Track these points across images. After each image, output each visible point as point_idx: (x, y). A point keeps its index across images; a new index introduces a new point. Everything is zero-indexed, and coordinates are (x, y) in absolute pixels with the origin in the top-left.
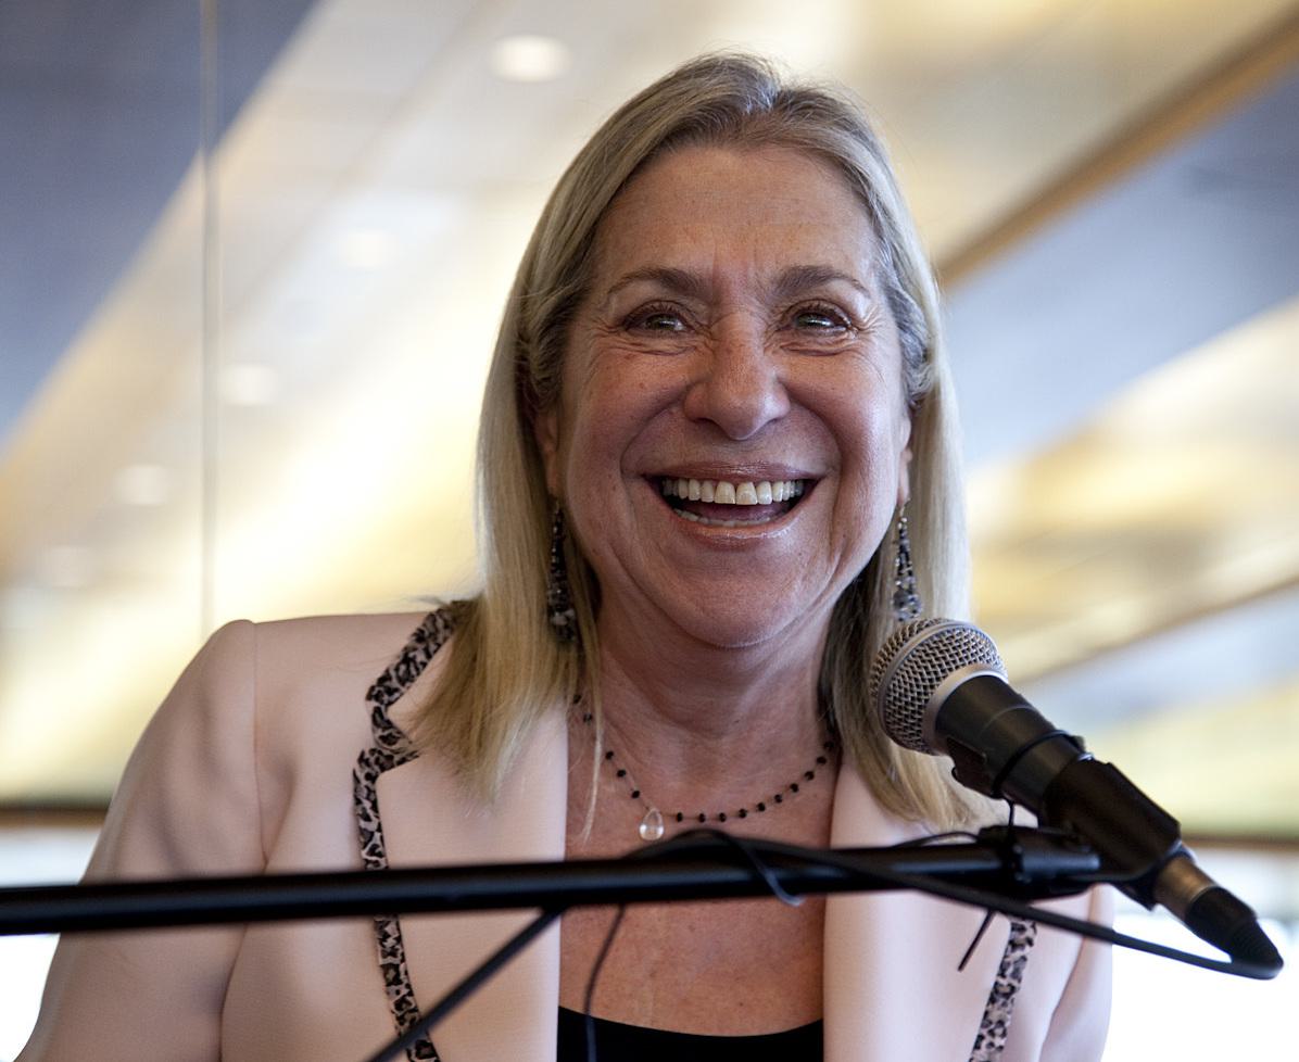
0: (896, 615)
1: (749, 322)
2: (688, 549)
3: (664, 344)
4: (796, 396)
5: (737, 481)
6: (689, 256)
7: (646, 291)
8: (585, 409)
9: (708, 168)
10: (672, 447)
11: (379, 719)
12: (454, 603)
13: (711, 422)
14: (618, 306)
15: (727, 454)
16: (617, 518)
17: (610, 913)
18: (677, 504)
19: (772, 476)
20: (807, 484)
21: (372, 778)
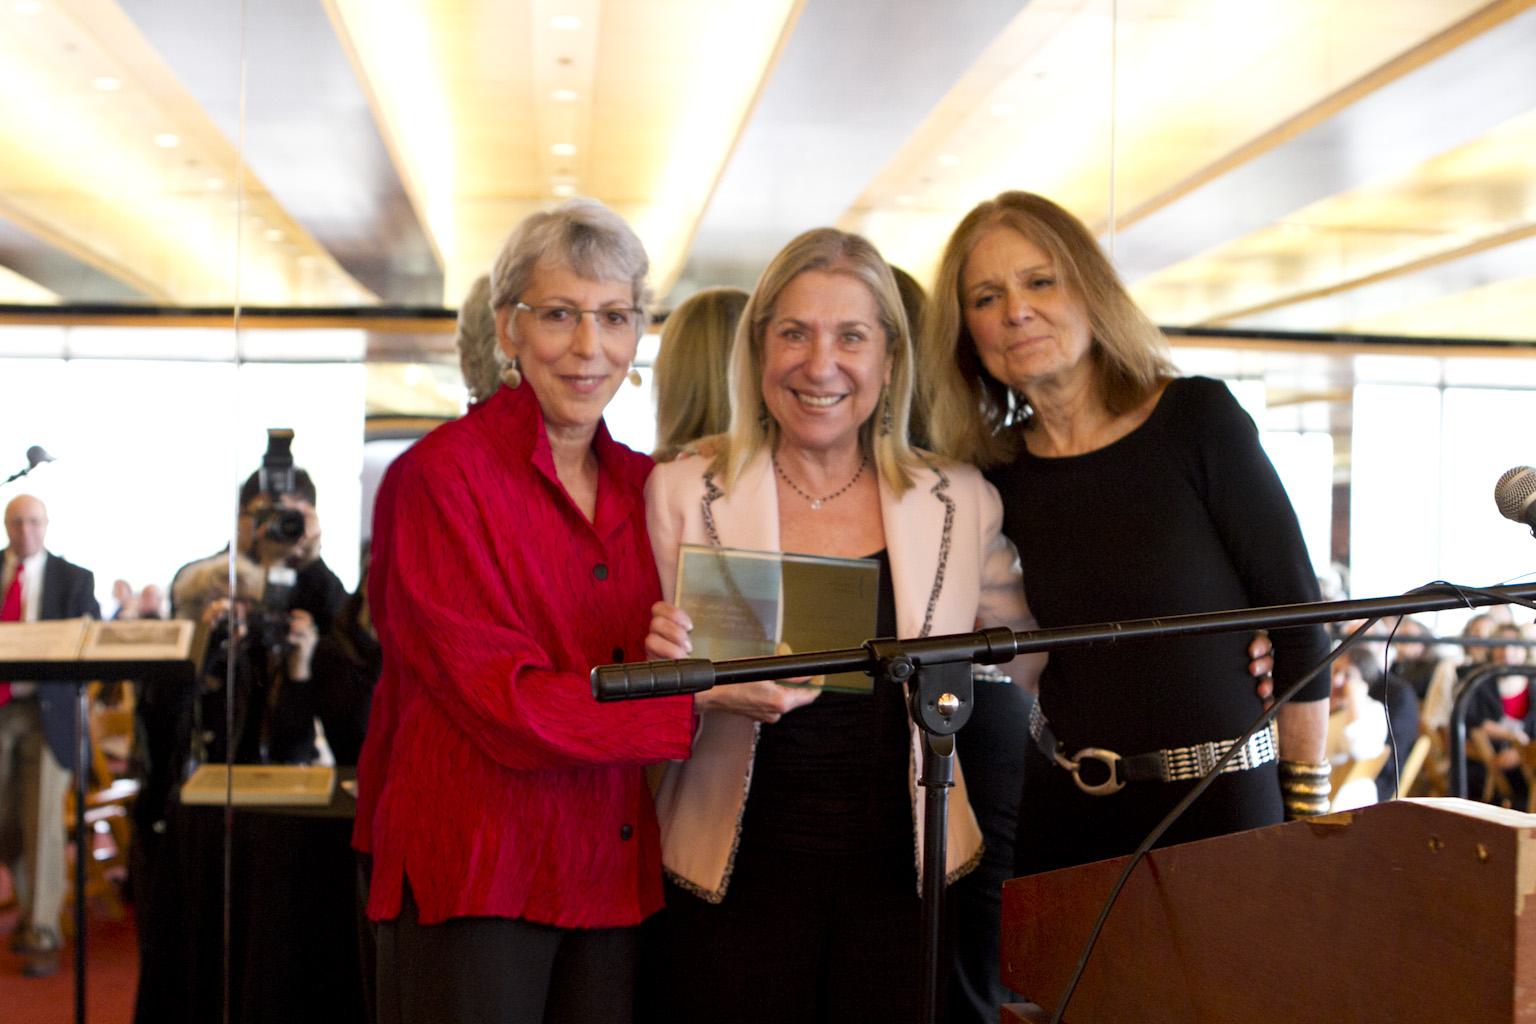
0: (883, 426)
1: (827, 340)
2: (800, 413)
3: (797, 345)
4: (841, 368)
5: (819, 397)
6: (805, 316)
7: (790, 325)
8: (770, 366)
9: (814, 285)
10: (798, 382)
11: (708, 484)
12: (1389, 741)
13: (180, 571)
14: (781, 328)
15: (815, 389)
16: (781, 404)
17: (933, 633)
18: (800, 402)
19: (829, 395)
20: (843, 397)
21: (708, 504)
